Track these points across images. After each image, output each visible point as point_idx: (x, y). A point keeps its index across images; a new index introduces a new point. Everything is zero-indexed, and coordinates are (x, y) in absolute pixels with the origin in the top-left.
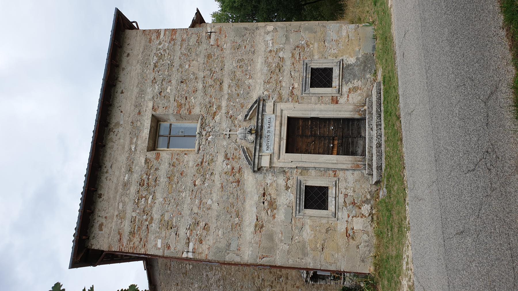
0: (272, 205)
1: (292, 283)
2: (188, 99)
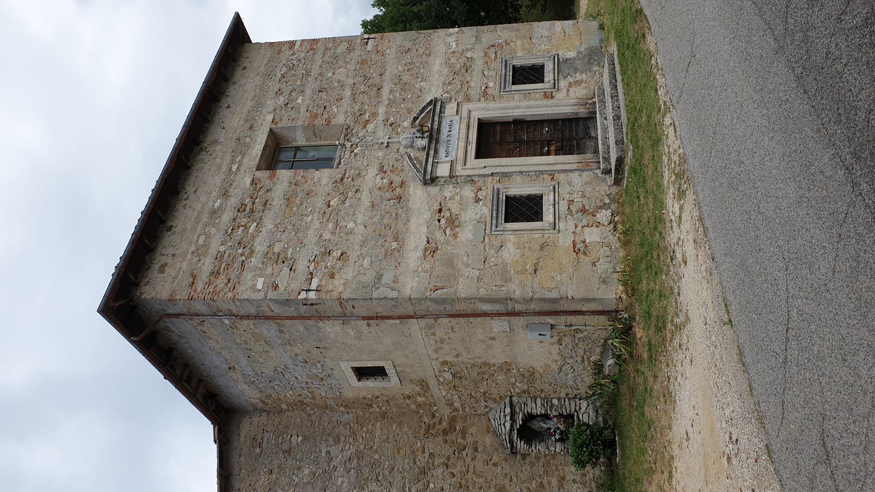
0: (453, 222)
1: (485, 456)
2: (328, 109)
